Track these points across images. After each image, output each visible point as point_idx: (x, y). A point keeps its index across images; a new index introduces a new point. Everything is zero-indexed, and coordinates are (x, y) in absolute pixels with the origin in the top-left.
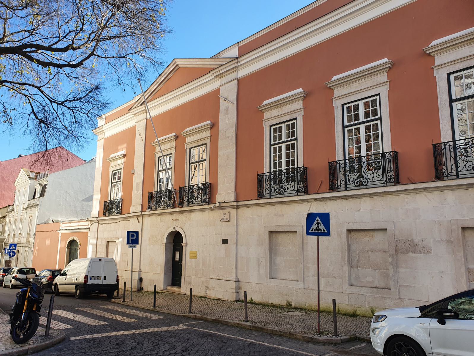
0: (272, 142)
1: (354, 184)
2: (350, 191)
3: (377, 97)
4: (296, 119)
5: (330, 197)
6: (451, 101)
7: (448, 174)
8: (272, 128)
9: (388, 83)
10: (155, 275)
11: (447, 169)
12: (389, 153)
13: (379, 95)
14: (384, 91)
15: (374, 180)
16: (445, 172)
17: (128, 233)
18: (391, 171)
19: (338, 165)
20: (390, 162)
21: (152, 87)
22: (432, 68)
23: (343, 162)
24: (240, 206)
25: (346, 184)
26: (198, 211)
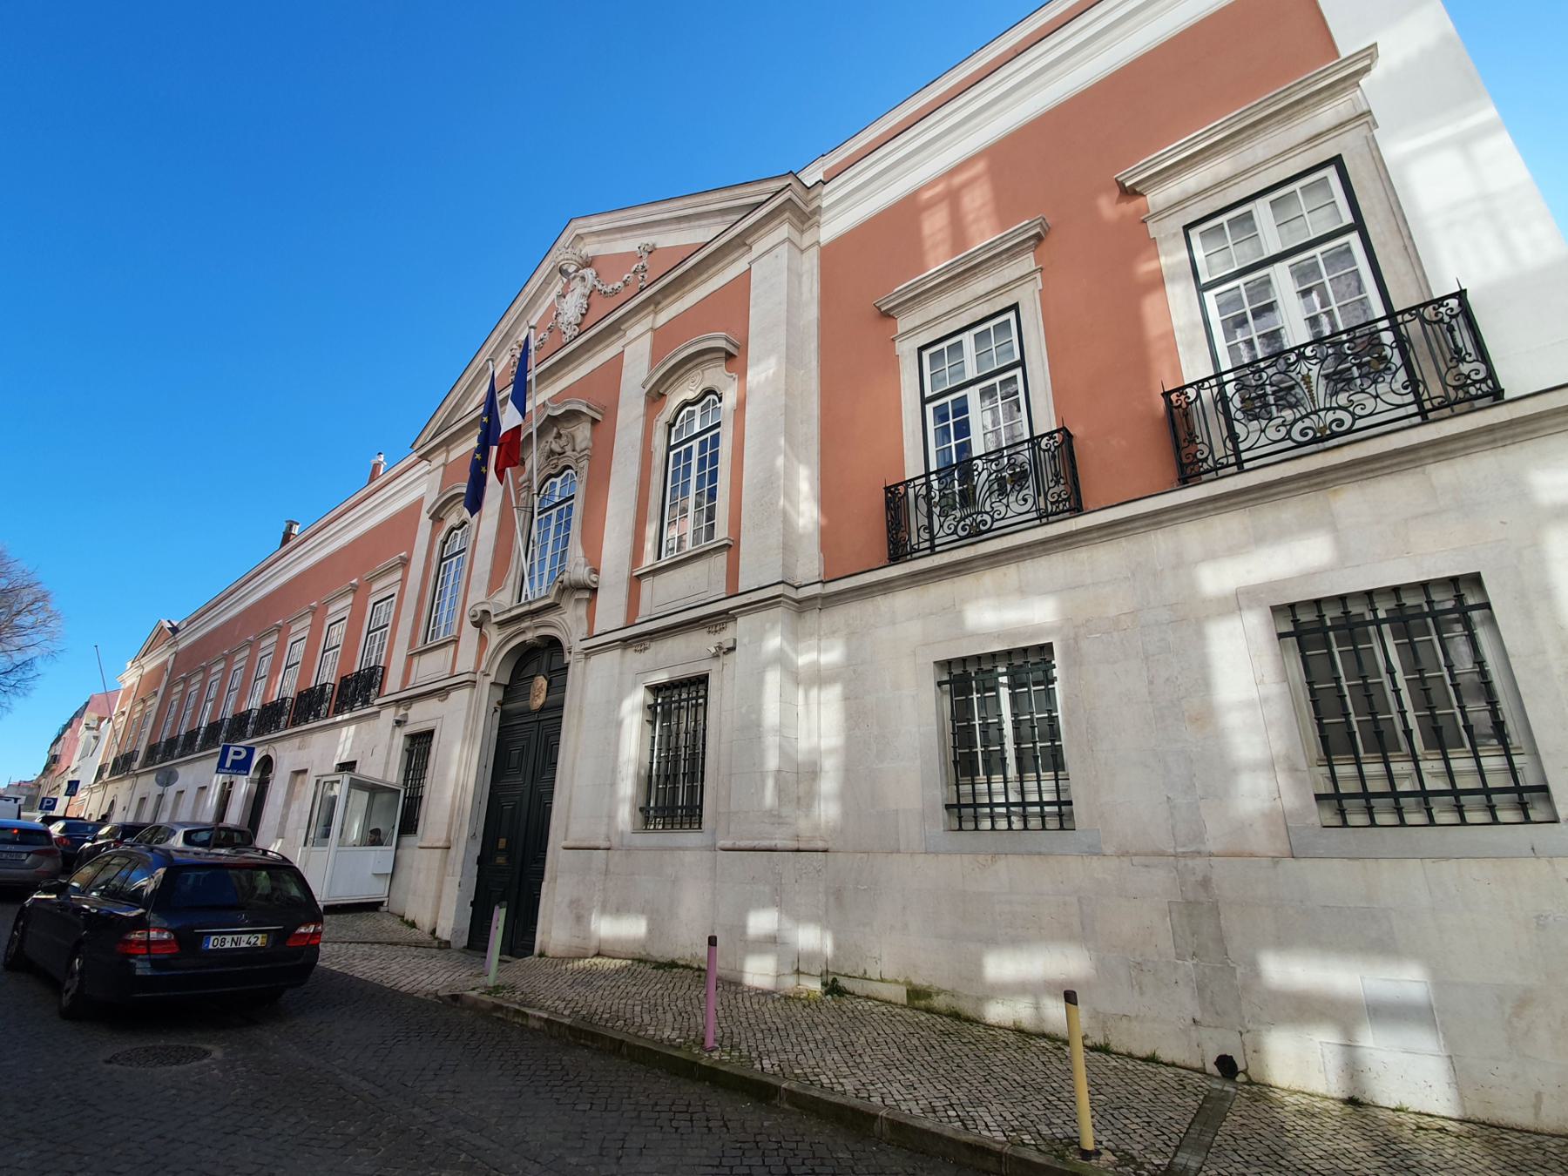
0: (928, 393)
1: (1290, 438)
2: (1252, 473)
3: (1011, 315)
4: (1015, 307)
5: (1029, 546)
6: (1359, 225)
7: (1215, 462)
8: (926, 355)
9: (1038, 275)
10: (434, 886)
11: (1211, 451)
12: (1050, 435)
13: (1015, 307)
14: (1029, 297)
15: (1010, 514)
16: (1206, 460)
17: (1476, 580)
18: (1057, 483)
19: (911, 491)
20: (1054, 457)
21: (738, 191)
22: (1144, 222)
23: (923, 480)
24: (1422, 453)
25: (932, 538)
26: (1466, 451)
